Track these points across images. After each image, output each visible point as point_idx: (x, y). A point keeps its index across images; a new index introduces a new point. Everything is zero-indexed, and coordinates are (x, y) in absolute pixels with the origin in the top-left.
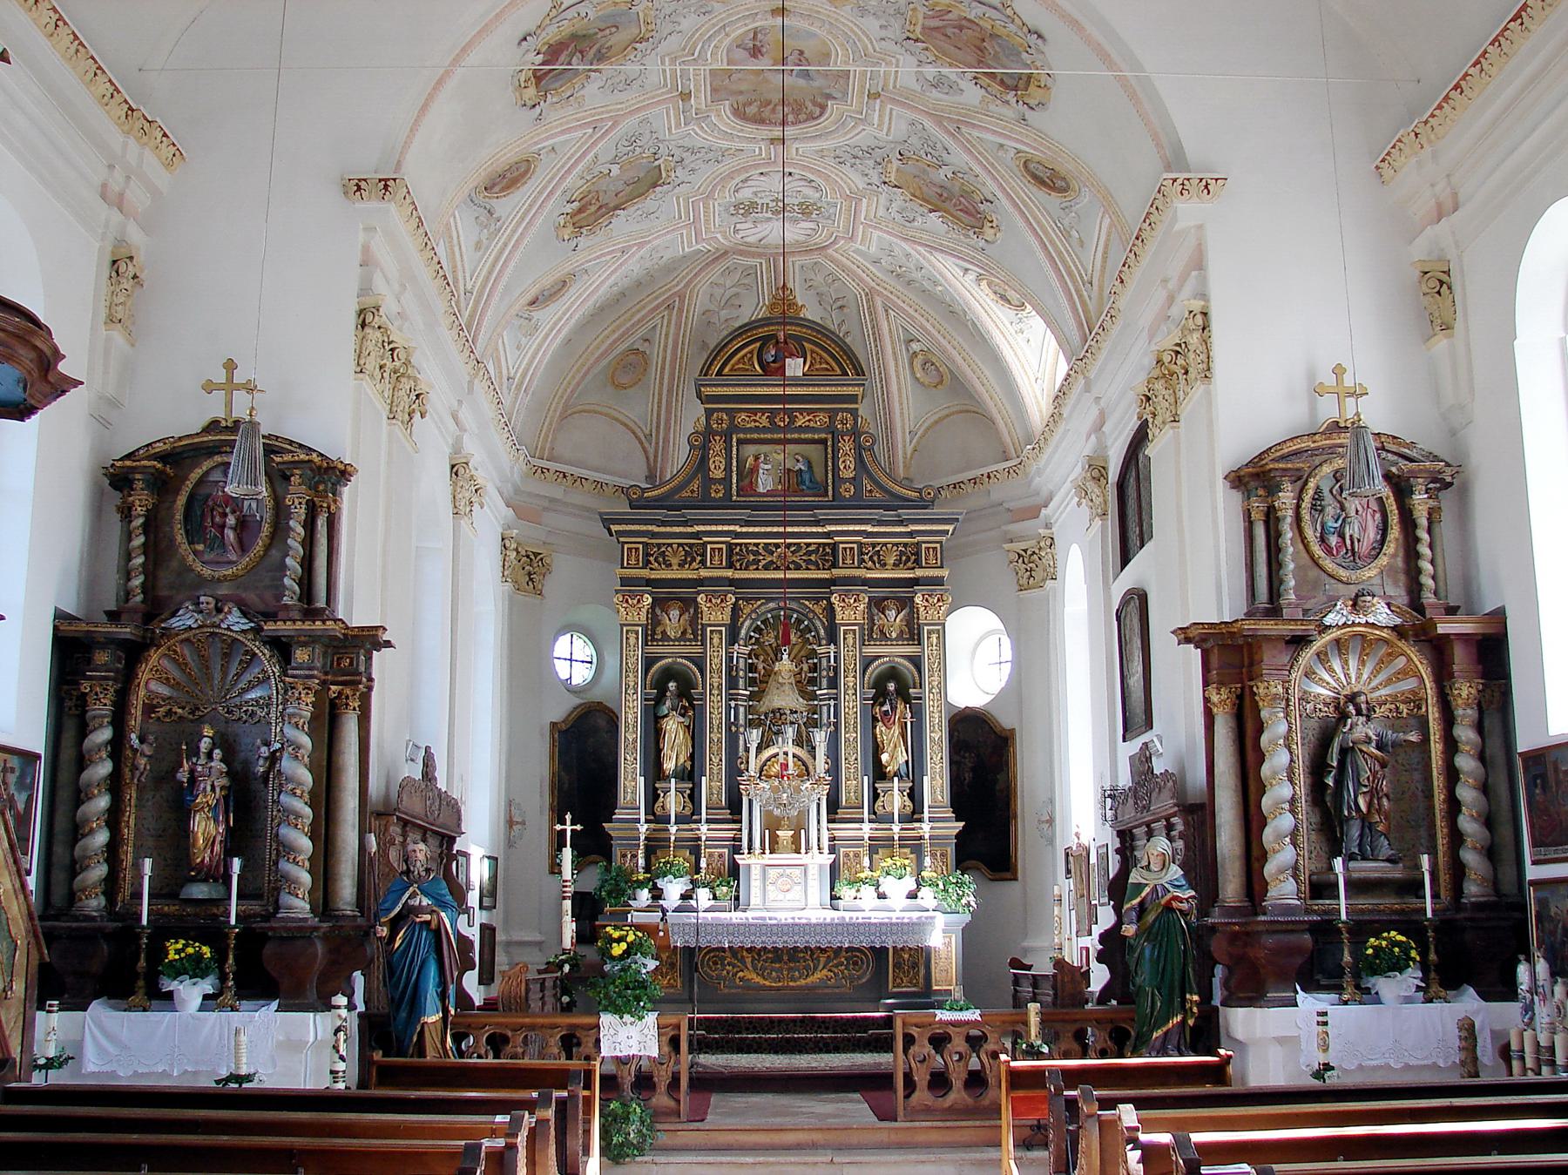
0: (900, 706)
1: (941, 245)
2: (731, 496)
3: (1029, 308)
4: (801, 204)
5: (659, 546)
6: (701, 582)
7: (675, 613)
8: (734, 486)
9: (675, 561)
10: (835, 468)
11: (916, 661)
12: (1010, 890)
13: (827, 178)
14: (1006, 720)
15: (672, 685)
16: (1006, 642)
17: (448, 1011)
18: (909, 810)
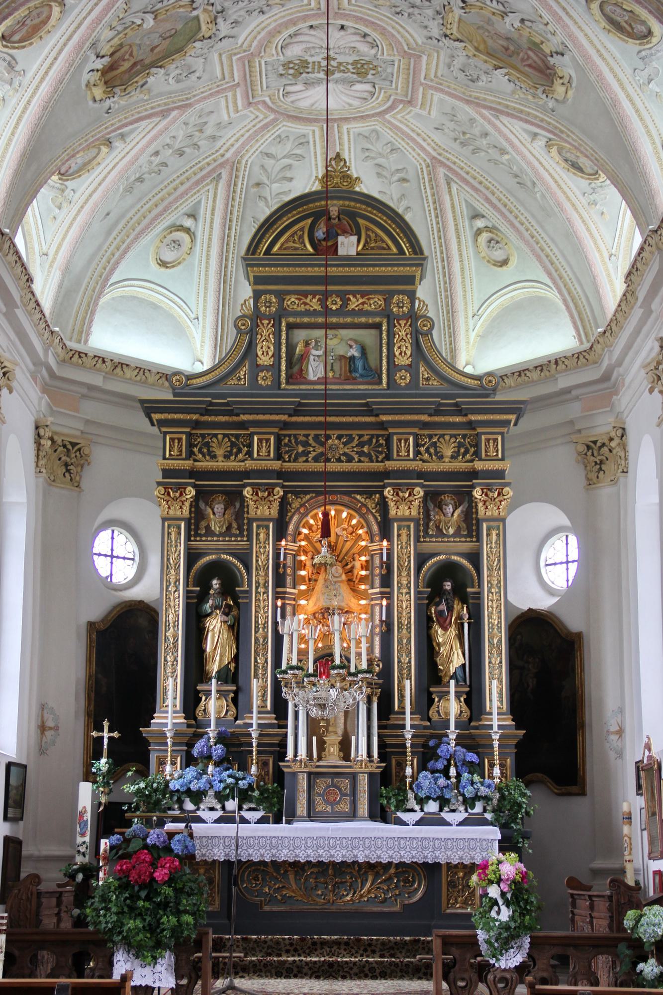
0: (457, 606)
1: (507, 106)
2: (280, 383)
3: (603, 177)
4: (355, 63)
5: (203, 436)
6: (247, 474)
7: (219, 508)
8: (283, 374)
9: (220, 452)
10: (391, 356)
11: (475, 558)
12: (577, 806)
13: (383, 32)
14: (573, 622)
15: (215, 583)
16: (573, 540)
18: (466, 714)
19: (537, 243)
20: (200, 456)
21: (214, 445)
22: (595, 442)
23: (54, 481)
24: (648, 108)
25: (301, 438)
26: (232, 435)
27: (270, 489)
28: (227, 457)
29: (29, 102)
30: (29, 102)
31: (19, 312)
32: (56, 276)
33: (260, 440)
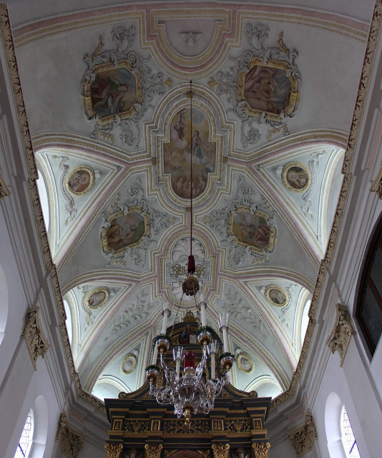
5: (130, 421)
17: (172, 335)
19: (262, 353)
20: (128, 430)
21: (134, 426)
22: (298, 434)
23: (64, 451)
24: (309, 223)
25: (172, 423)
26: (142, 421)
27: (157, 445)
28: (139, 431)
29: (76, 226)
30: (76, 226)
31: (57, 329)
32: (82, 356)
33: (154, 423)
